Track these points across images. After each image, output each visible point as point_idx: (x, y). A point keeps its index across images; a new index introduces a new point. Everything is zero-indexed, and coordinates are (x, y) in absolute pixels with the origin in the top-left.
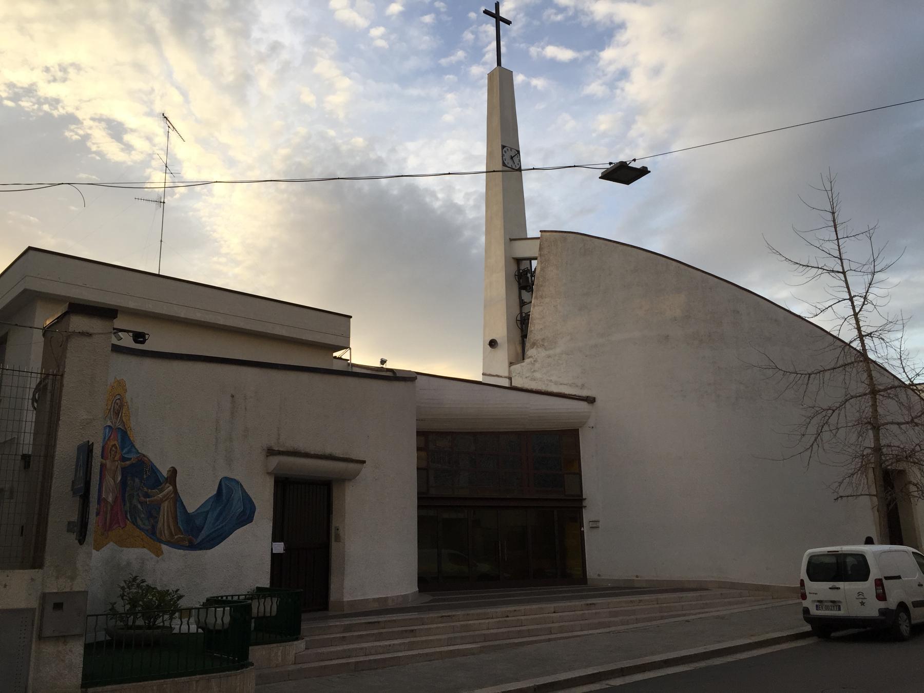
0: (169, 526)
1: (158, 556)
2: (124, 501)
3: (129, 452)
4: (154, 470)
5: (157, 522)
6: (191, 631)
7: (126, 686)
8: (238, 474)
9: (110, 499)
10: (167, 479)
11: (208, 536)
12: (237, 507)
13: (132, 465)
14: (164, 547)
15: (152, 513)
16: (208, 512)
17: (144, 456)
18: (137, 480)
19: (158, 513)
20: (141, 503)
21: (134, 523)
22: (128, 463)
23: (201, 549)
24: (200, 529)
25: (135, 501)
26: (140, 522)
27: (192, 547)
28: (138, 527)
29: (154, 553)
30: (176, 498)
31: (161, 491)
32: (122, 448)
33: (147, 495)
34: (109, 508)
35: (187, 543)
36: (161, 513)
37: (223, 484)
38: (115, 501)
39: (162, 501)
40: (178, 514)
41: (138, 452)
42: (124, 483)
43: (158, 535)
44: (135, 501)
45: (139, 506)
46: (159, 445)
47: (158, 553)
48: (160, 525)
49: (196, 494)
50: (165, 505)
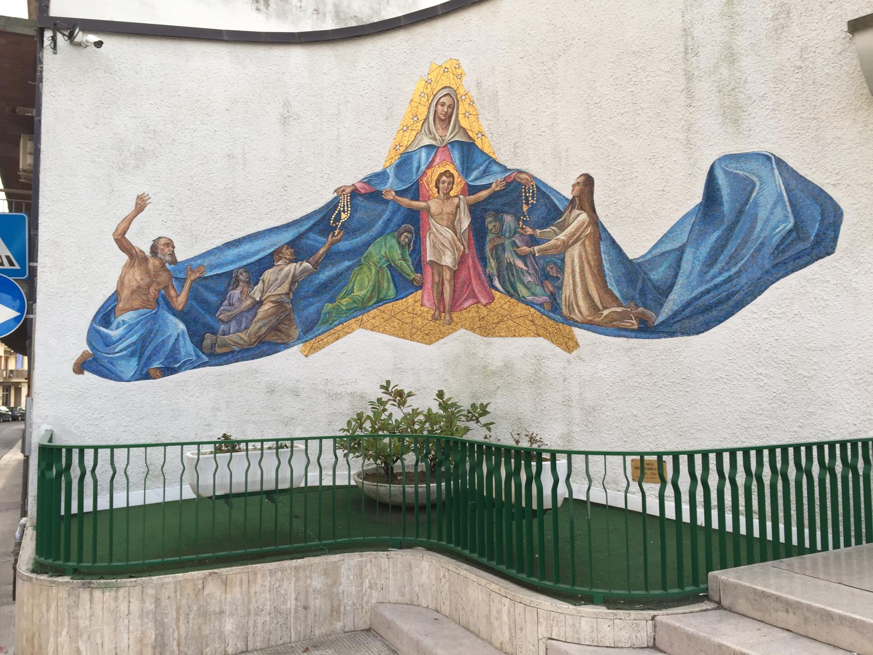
0: (587, 295)
1: (569, 350)
2: (483, 260)
3: (485, 173)
4: (543, 192)
5: (560, 288)
6: (324, 483)
7: (287, 563)
8: (766, 133)
9: (448, 260)
10: (572, 201)
11: (688, 304)
12: (772, 218)
13: (495, 195)
14: (578, 332)
15: (550, 272)
16: (681, 250)
17: (520, 172)
18: (508, 219)
19: (562, 270)
20: (523, 258)
21: (512, 292)
22: (484, 194)
23: (672, 334)
24: (665, 291)
25: (508, 256)
26: (523, 291)
27: (646, 330)
28: (522, 300)
29: (559, 345)
30: (599, 232)
31: (562, 228)
32: (466, 170)
33: (533, 241)
34: (447, 275)
35: (634, 324)
36: (568, 269)
37: (722, 180)
38: (461, 261)
39: (566, 246)
40: (606, 266)
41: (506, 169)
42: (478, 231)
43: (565, 310)
44: (508, 256)
45: (520, 264)
46: (538, 147)
47: (570, 345)
48: (567, 291)
49: (645, 213)
50: (574, 253)
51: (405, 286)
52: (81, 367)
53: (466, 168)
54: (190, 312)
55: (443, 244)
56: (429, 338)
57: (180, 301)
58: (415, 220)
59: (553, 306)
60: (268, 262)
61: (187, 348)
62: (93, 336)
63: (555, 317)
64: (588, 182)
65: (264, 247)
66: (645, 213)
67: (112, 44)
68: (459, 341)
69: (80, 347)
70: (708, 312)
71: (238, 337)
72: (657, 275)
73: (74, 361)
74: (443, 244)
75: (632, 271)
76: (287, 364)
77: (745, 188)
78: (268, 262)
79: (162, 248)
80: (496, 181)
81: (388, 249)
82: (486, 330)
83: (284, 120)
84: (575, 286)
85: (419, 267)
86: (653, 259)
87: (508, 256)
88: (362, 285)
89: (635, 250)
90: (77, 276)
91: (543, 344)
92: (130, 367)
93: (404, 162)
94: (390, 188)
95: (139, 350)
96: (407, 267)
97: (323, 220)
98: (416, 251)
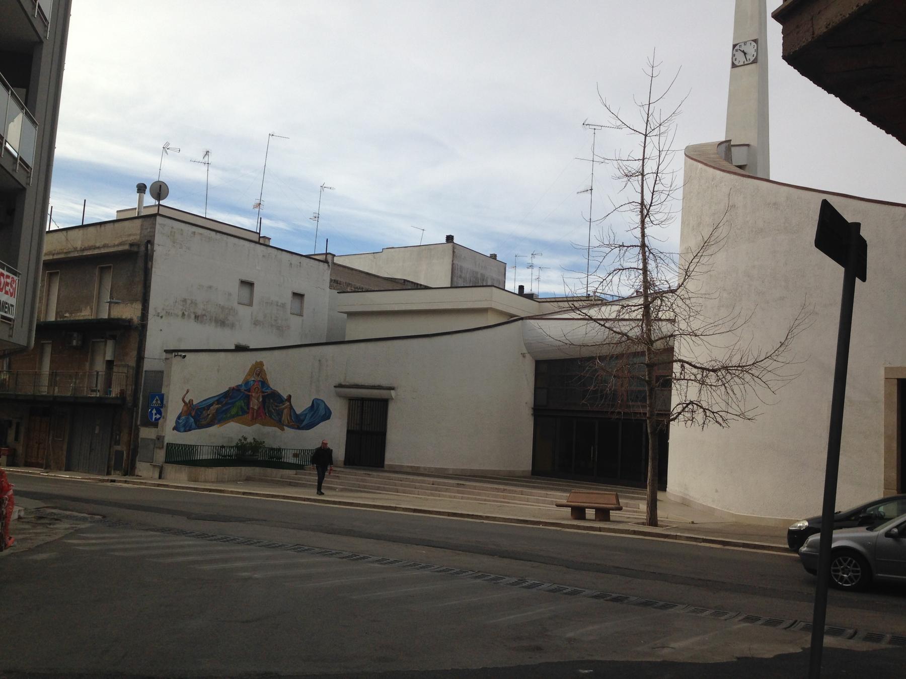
4: (279, 396)
12: (322, 412)
15: (280, 413)
21: (270, 417)
27: (299, 428)
30: (291, 408)
38: (259, 408)
42: (264, 401)
46: (280, 383)
47: (283, 430)
49: (301, 405)
50: (285, 411)
51: (244, 412)
52: (174, 429)
53: (263, 387)
54: (196, 416)
55: (255, 404)
56: (249, 425)
57: (193, 414)
58: (248, 398)
59: (280, 421)
60: (212, 405)
61: (194, 425)
62: (177, 422)
63: (280, 425)
64: (290, 397)
65: (211, 401)
66: (301, 405)
67: (188, 355)
68: (257, 426)
69: (174, 424)
70: (309, 426)
71: (204, 422)
72: (302, 418)
73: (512, 469)
74: (255, 404)
75: (297, 416)
76: (214, 429)
77: (318, 405)
78: (212, 405)
79: (191, 401)
80: (269, 391)
81: (241, 403)
82: (264, 424)
83: (218, 371)
84: (285, 417)
85: (248, 408)
86: (301, 415)
87: (271, 409)
88: (234, 411)
89: (298, 413)
90: (174, 409)
91: (276, 429)
92: (182, 429)
93: (246, 383)
94: (243, 388)
95: (184, 426)
96: (245, 408)
97: (226, 395)
98: (248, 405)
